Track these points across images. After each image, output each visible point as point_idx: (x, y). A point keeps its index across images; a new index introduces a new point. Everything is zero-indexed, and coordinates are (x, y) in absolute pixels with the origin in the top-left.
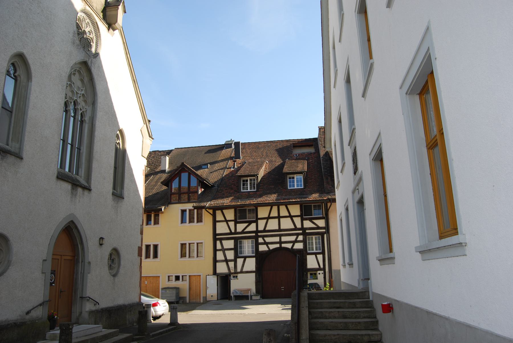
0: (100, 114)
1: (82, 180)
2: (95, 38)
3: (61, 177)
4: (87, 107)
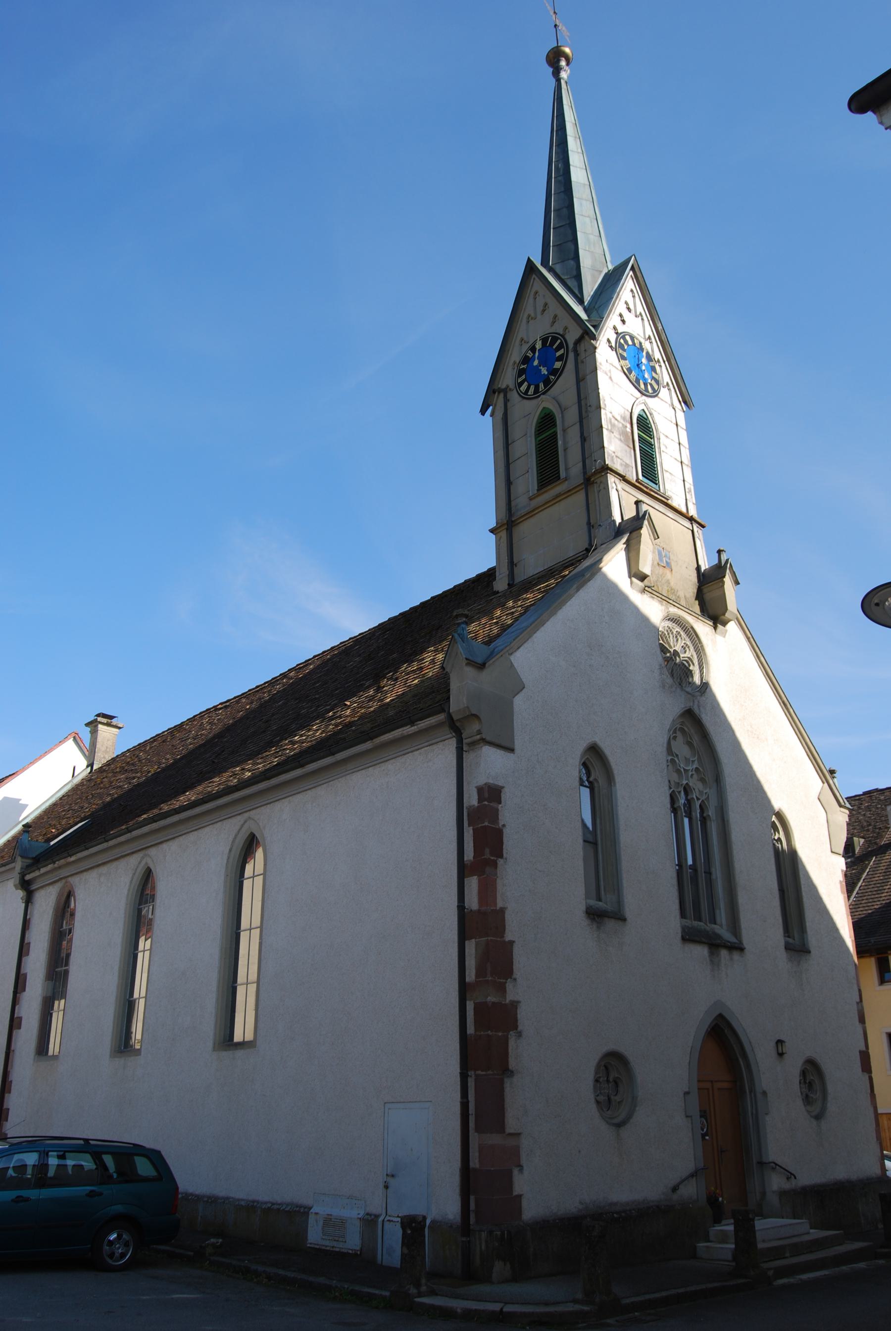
1: (727, 936)
2: (695, 656)
3: (689, 937)
4: (707, 790)
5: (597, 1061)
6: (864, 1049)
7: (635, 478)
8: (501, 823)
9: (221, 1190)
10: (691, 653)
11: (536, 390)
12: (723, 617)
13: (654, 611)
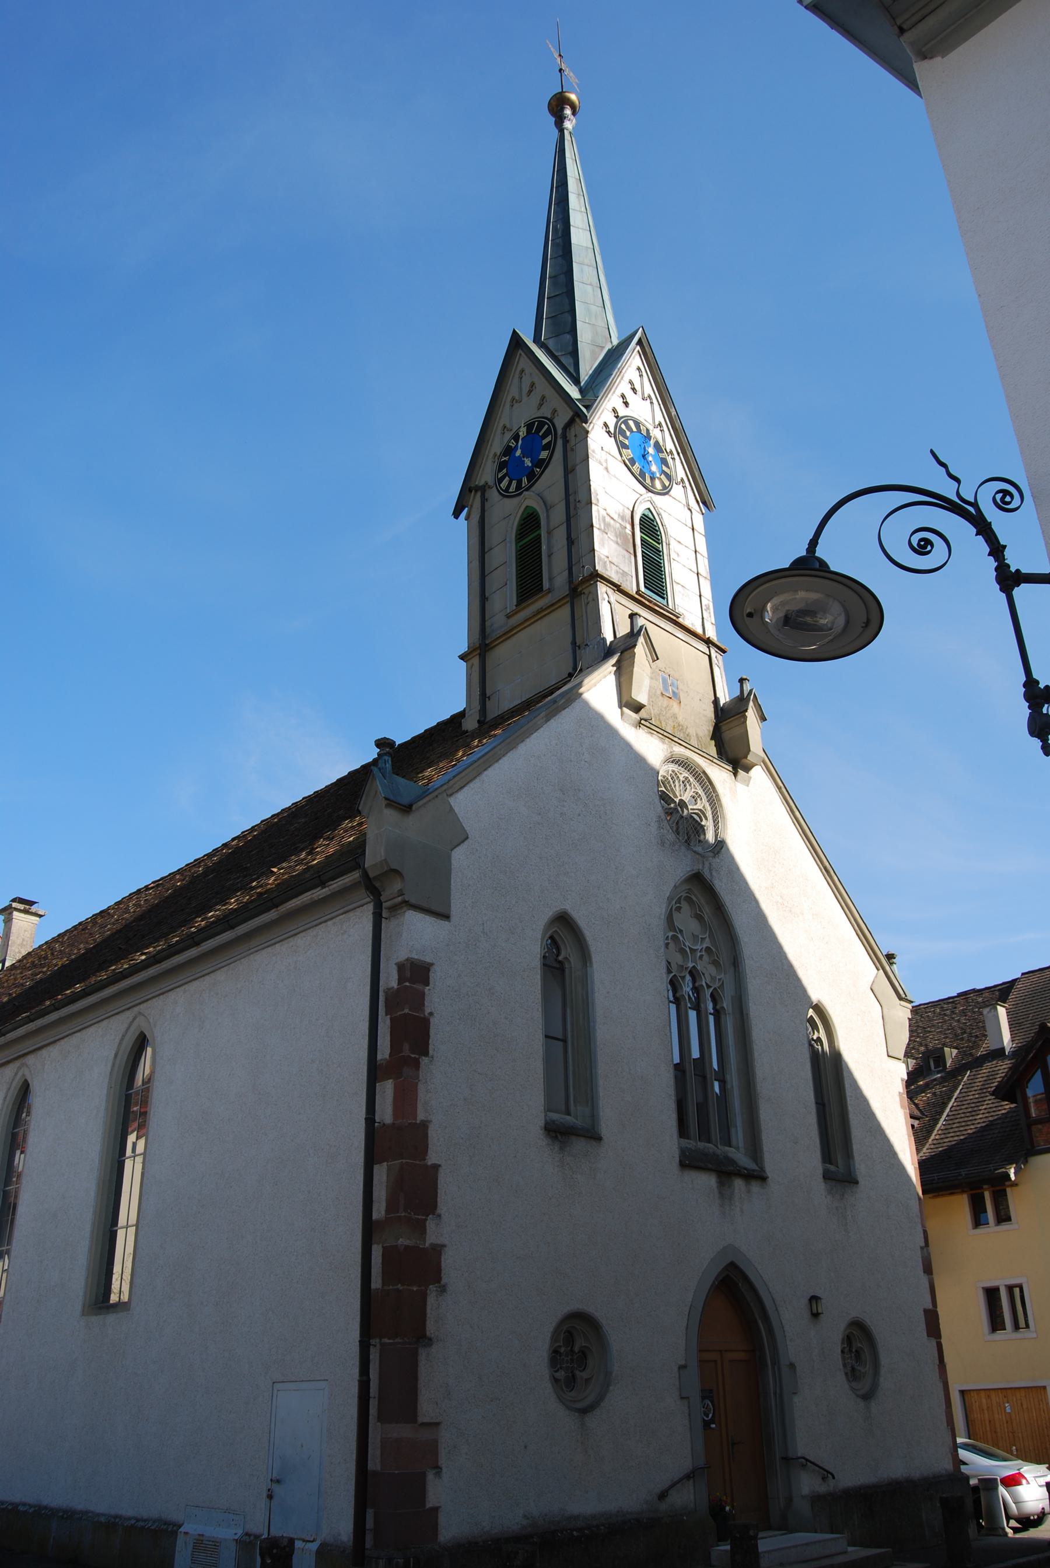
0: (754, 985)
1: (743, 1160)
3: (689, 1162)
4: (722, 976)
5: (554, 1324)
6: (931, 1307)
7: (635, 589)
8: (427, 1011)
9: (79, 1502)
10: (703, 804)
11: (519, 486)
12: (744, 761)
13: (653, 750)
